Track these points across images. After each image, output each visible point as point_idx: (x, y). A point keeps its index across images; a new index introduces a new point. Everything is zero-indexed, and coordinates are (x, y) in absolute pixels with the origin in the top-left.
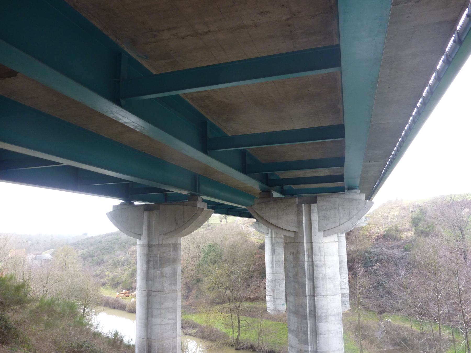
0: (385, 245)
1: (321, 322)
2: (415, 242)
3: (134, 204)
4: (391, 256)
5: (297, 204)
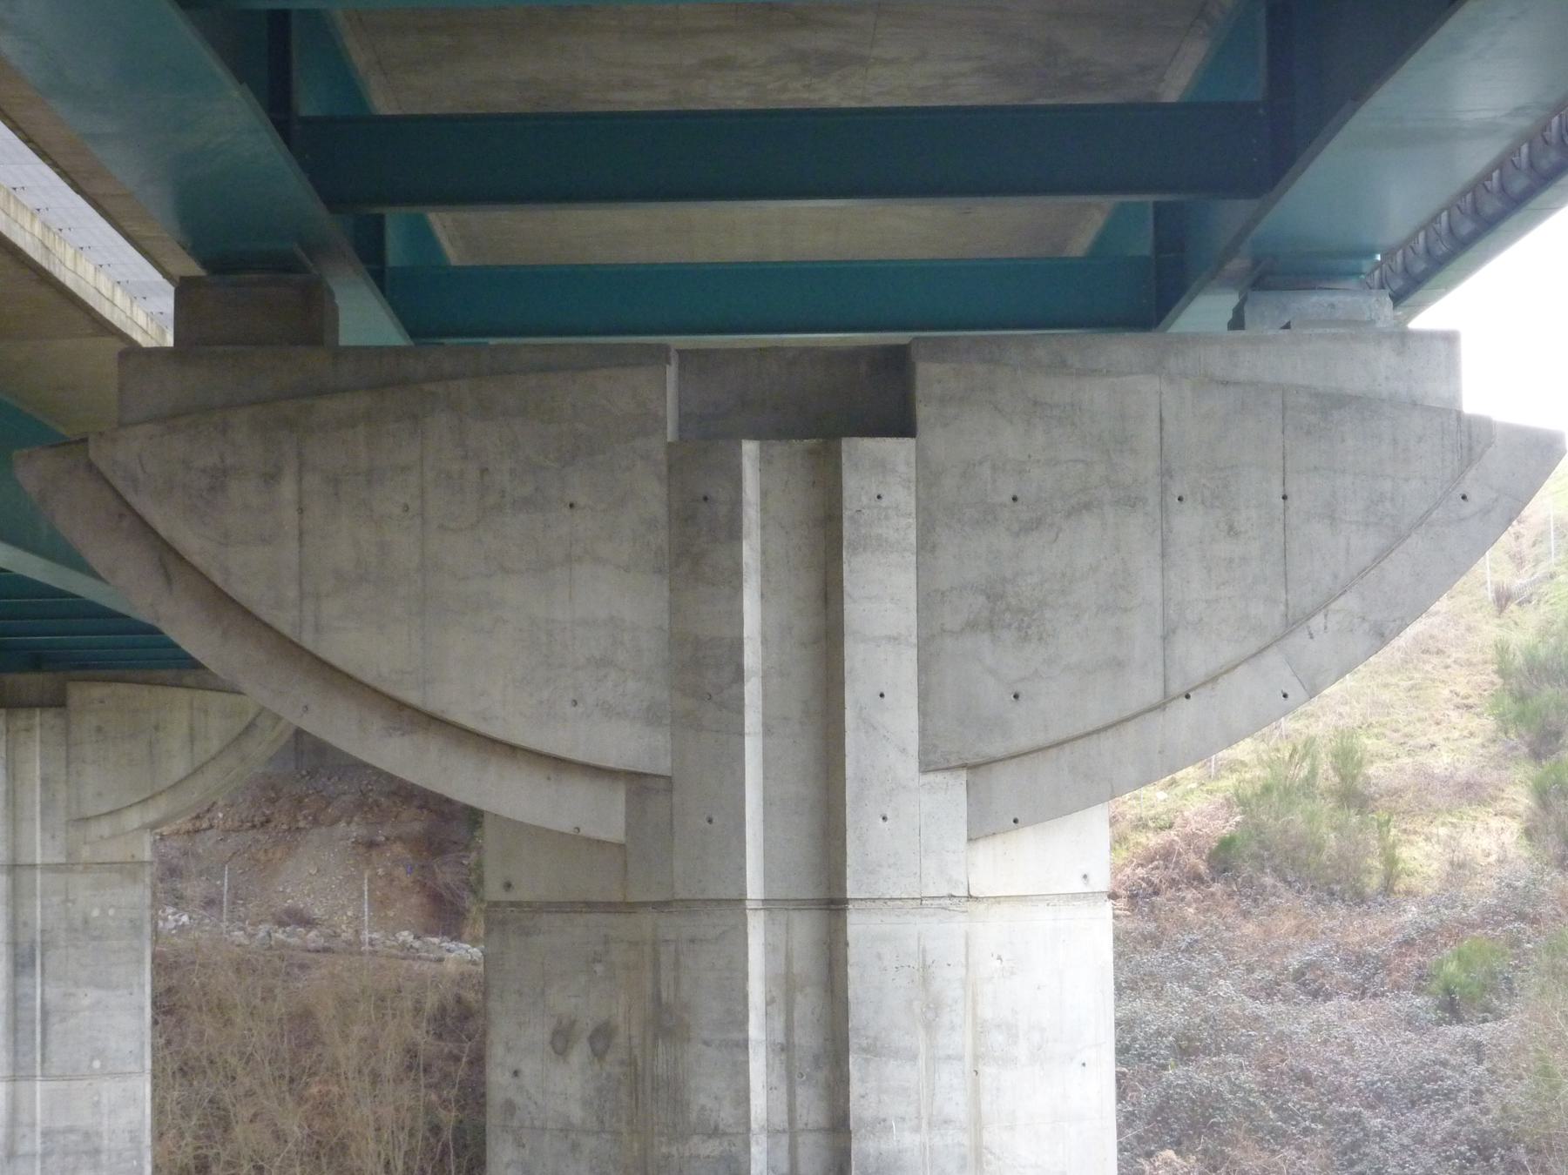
0: (1229, 955)
2: (1534, 921)
4: (1303, 1064)
5: (669, 440)
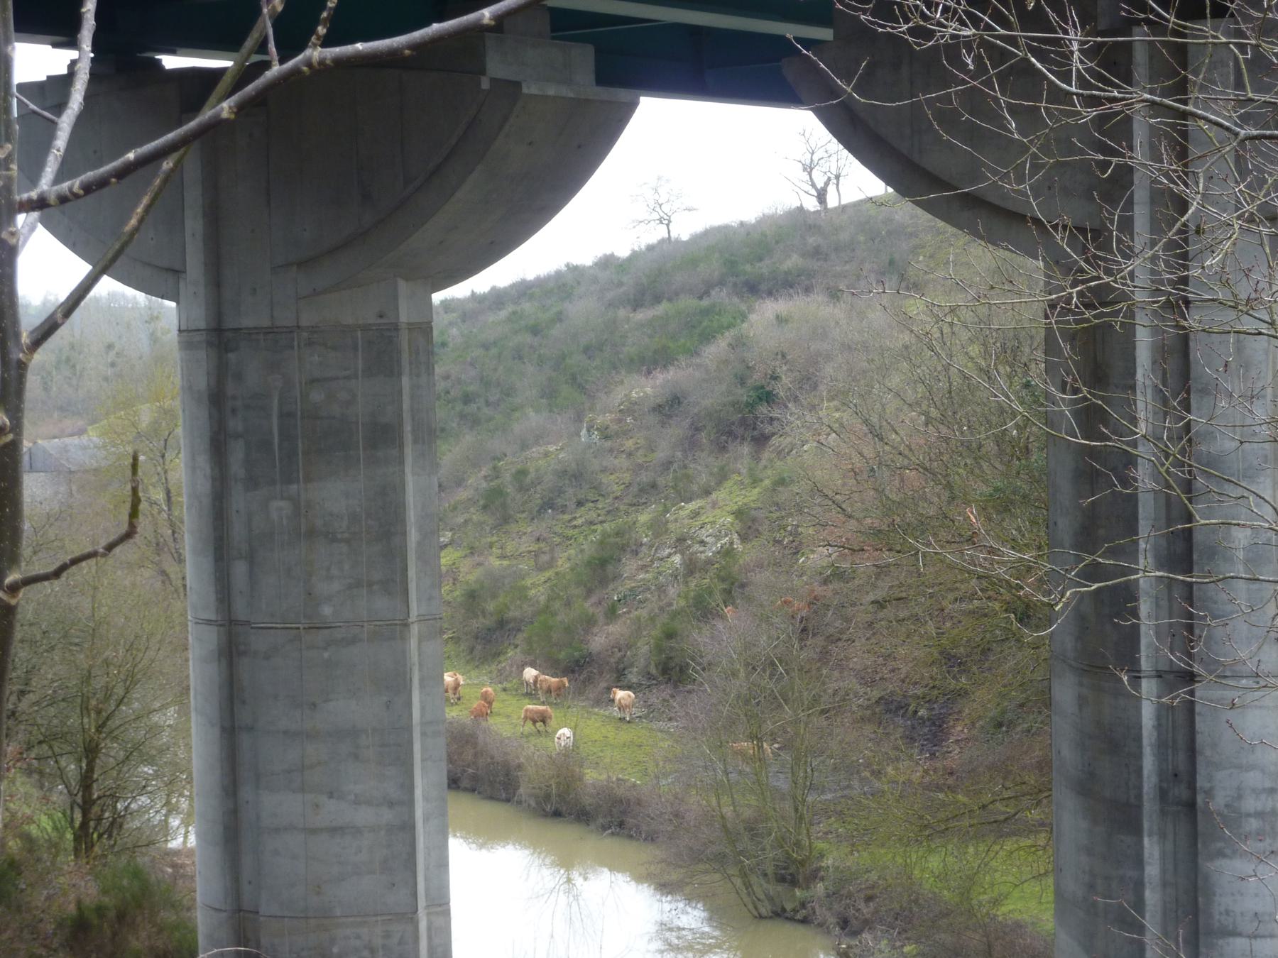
1: (1228, 851)
3: (163, 67)
